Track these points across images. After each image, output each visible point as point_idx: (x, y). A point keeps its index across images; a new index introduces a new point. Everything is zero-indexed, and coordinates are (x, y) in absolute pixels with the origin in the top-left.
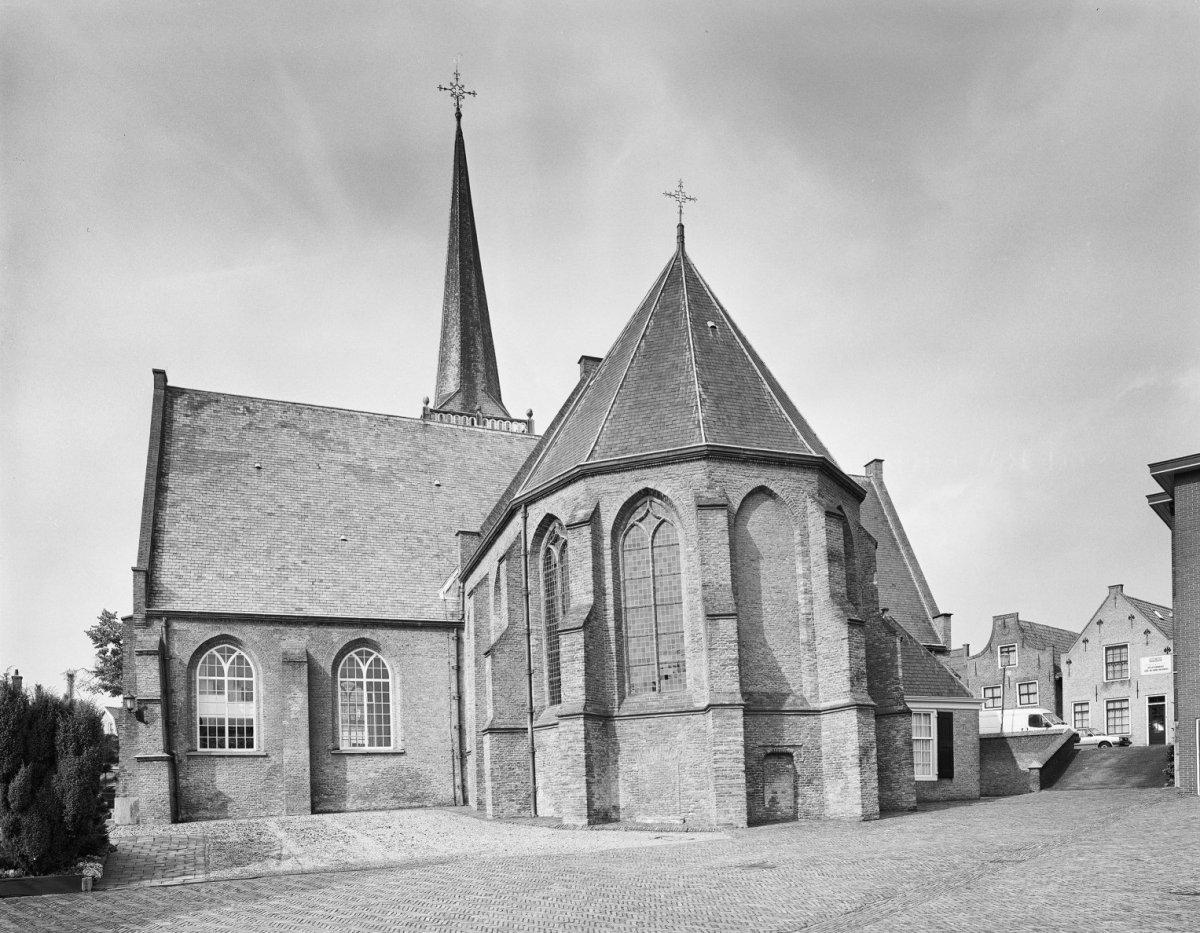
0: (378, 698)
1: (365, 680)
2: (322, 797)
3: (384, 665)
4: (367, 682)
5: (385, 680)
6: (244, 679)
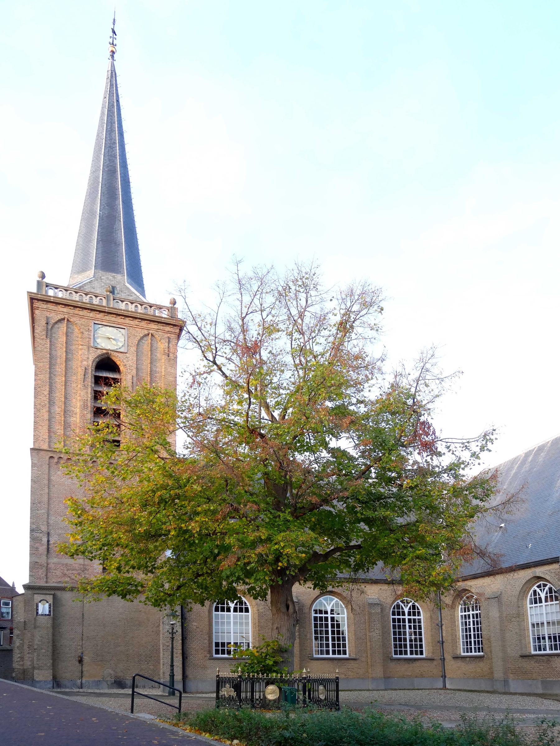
1: (407, 617)
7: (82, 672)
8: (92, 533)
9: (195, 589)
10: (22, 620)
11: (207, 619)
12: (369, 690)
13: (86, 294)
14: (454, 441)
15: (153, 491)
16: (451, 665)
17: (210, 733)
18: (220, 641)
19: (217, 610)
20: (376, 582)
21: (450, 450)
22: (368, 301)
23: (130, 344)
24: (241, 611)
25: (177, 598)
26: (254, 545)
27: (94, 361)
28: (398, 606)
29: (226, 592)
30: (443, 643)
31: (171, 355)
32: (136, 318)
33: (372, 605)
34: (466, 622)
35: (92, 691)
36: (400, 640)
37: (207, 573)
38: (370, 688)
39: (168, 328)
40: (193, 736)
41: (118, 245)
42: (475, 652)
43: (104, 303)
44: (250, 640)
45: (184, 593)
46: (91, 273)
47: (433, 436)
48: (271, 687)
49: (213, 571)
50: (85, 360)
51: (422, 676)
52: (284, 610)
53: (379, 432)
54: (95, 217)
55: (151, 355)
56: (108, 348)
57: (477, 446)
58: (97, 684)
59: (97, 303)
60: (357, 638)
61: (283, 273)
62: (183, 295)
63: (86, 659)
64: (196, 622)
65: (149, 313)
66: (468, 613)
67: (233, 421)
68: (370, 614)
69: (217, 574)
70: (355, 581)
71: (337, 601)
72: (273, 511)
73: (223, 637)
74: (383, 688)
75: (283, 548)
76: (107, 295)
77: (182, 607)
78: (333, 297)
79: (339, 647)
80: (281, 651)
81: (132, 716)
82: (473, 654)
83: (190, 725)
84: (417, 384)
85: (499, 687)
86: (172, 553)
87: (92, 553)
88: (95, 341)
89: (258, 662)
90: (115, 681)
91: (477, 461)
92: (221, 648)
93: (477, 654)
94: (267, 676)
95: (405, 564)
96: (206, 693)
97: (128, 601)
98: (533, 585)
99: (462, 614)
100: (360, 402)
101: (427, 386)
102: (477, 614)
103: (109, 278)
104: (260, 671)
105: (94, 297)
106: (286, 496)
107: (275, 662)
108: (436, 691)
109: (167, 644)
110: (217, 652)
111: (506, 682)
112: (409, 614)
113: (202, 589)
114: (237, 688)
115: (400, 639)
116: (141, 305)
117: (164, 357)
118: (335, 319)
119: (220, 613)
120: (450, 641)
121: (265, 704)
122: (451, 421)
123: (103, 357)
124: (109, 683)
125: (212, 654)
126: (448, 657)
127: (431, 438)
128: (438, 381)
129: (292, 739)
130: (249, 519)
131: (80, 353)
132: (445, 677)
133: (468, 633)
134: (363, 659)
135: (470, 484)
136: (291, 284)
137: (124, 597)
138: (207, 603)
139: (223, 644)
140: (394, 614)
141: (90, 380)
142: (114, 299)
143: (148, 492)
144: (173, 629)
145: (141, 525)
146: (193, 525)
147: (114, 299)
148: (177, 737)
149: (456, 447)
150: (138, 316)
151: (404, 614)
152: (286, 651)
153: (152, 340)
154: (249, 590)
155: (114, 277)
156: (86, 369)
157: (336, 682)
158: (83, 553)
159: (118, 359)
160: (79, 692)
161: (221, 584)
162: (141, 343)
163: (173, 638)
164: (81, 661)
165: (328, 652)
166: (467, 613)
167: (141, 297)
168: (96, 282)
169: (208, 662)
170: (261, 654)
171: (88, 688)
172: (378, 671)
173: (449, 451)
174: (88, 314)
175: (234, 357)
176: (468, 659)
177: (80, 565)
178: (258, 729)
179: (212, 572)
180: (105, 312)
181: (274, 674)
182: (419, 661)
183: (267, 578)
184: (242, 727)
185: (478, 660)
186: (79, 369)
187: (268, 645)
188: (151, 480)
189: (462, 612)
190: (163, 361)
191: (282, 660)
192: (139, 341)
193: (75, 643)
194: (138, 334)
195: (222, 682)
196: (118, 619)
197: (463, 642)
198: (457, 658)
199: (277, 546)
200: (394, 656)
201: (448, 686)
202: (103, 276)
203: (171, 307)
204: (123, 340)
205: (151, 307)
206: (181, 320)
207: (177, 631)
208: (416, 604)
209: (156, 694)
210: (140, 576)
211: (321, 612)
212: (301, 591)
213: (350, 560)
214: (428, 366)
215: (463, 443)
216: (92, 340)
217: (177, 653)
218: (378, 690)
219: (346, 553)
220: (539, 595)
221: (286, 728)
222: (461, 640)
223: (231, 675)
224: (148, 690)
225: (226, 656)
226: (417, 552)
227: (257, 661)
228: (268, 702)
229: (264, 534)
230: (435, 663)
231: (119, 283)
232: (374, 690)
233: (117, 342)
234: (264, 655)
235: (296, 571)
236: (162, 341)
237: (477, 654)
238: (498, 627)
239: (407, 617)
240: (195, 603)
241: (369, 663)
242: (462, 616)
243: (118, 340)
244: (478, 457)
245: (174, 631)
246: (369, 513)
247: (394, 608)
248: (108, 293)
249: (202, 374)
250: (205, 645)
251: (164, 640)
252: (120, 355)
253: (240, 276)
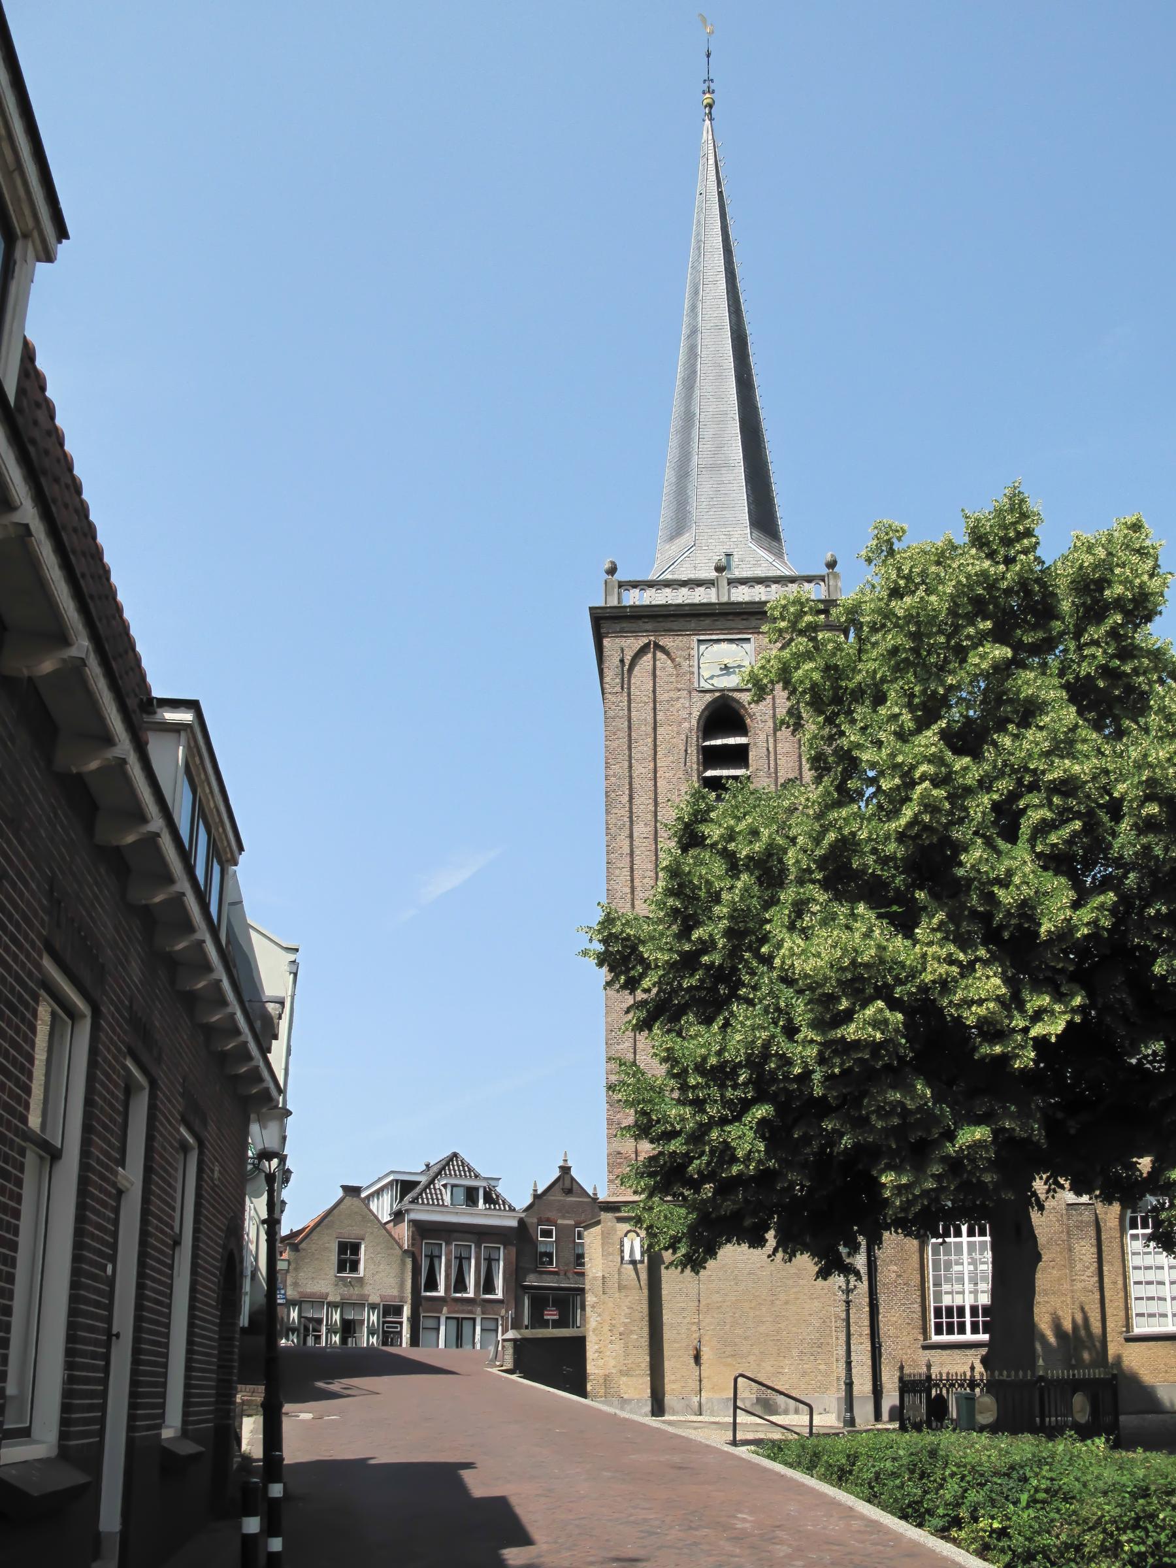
7: (700, 1381)
10: (600, 1274)
27: (700, 716)
90: (758, 1399)
164: (697, 1358)
165: (962, 1330)
193: (688, 1320)
196: (758, 1265)
216: (696, 675)
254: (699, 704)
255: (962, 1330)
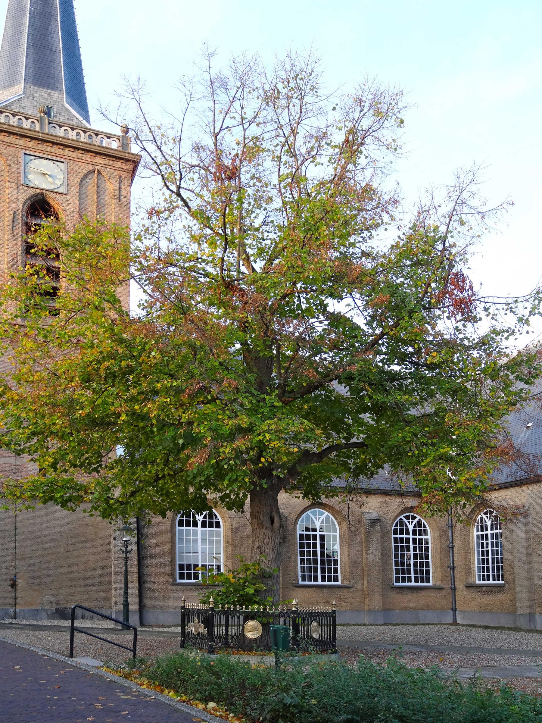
0: (421, 549)
1: (411, 536)
2: (71, 656)
3: (425, 527)
4: (320, 535)
5: (425, 537)
6: (331, 533)
7: (15, 599)
8: (19, 417)
9: (154, 496)
11: (169, 536)
12: (365, 625)
13: (14, 115)
14: (496, 300)
15: (98, 362)
16: (463, 596)
17: (175, 692)
18: (185, 563)
19: (181, 524)
20: (376, 492)
21: (489, 314)
22: (383, 109)
23: (71, 183)
24: (211, 526)
25: (131, 507)
26: (231, 437)
27: (25, 203)
28: (401, 523)
29: (193, 500)
30: (454, 569)
31: (123, 199)
32: (78, 149)
33: (370, 521)
34: (483, 544)
35: (28, 623)
36: (403, 564)
37: (169, 475)
38: (367, 623)
39: (118, 164)
40: (152, 694)
41: (54, 52)
42: (494, 580)
43: (37, 127)
44: (222, 561)
45: (140, 501)
46: (19, 88)
47: (470, 292)
48: (251, 623)
49: (176, 472)
50: (13, 202)
51: (428, 608)
52: (268, 524)
53: (394, 289)
54: (25, 15)
55: (97, 198)
56: (42, 187)
57: (526, 308)
58: (35, 613)
59: (28, 127)
60: (352, 562)
61: (270, 71)
62: (137, 98)
63: (20, 583)
64: (155, 539)
65: (95, 143)
66: (486, 532)
67: (204, 270)
68: (368, 532)
69: (182, 476)
70: (352, 491)
71: (327, 515)
72: (256, 393)
73: (188, 558)
74: (382, 622)
75: (270, 440)
76: (41, 117)
77: (138, 518)
78: (337, 105)
79: (330, 571)
80: (264, 576)
81: (69, 661)
82: (491, 582)
83: (148, 679)
84: (450, 220)
85: (523, 623)
86: (124, 451)
87: (20, 445)
88: (25, 176)
89: (236, 591)
91: (526, 328)
92: (188, 570)
93: (496, 582)
94: (247, 608)
95: (424, 466)
96: (169, 626)
97: (68, 510)
98: (480, 511)
99: (478, 533)
100: (366, 255)
101: (462, 223)
102: (497, 534)
103: (42, 96)
104: (237, 601)
105: (24, 119)
106: (271, 373)
107: (256, 591)
108: (446, 627)
109: (120, 566)
110: (181, 576)
111: (531, 617)
112: (414, 533)
113: (162, 495)
114: (208, 622)
115: (404, 563)
116: (85, 132)
117: (114, 202)
118: (339, 138)
119: (185, 528)
120: (463, 567)
121: (245, 645)
122: (493, 270)
123: (37, 198)
124: (49, 613)
125: (176, 578)
126: (460, 586)
127: (466, 295)
128: (479, 217)
129: (294, 706)
130: (224, 402)
131: (7, 192)
132: (456, 609)
133: (485, 557)
134: (359, 587)
135: (513, 360)
136: (280, 86)
137: (64, 504)
138: (169, 514)
139: (189, 566)
140: (396, 533)
141: (19, 228)
142: (49, 123)
143: (91, 362)
144: (127, 547)
145: (82, 408)
146: (150, 406)
147: (49, 123)
148: (129, 697)
149: (498, 309)
150: (81, 146)
151: (408, 533)
152: (270, 577)
153: (98, 179)
154: (222, 499)
155: (49, 94)
156: (14, 213)
157: (333, 617)
158: (8, 445)
159: (55, 202)
160: (11, 624)
161: (187, 490)
162: (85, 182)
163: (126, 559)
164: (13, 585)
165: (316, 579)
166: (484, 533)
167: (84, 122)
168: (26, 101)
169: (170, 588)
170: (238, 580)
171: (24, 618)
172: (377, 602)
173: (488, 315)
174: (17, 141)
175: (205, 192)
176: (484, 589)
177: (11, 465)
178: (242, 686)
179: (175, 474)
180: (37, 139)
181: (256, 607)
182: (426, 590)
183: (247, 480)
184: (220, 684)
185: (497, 590)
186: (7, 213)
187: (247, 569)
188: (95, 346)
189: (478, 531)
190: (113, 206)
191: (265, 588)
192: (83, 179)
193: (7, 563)
194: (80, 170)
195: (189, 615)
196: (59, 534)
197: (479, 568)
198: (471, 587)
199: (261, 437)
200: (395, 584)
201: (459, 621)
202: (36, 92)
203: (123, 136)
204: (62, 177)
205: (97, 135)
206: (137, 155)
207: (132, 550)
208: (423, 521)
209: (106, 627)
210: (83, 478)
211: (308, 529)
212: (288, 501)
213: (349, 462)
214: (465, 195)
215: (508, 304)
216: (22, 175)
217: (132, 577)
218: (376, 625)
219: (345, 453)
220: (486, 522)
221: (286, 690)
222: (476, 566)
223: (201, 606)
224: (97, 622)
225: (192, 581)
226: (441, 450)
227: (234, 589)
228: (247, 642)
229: (244, 420)
230: (444, 592)
231: (56, 102)
232: (371, 625)
233: (54, 180)
234: (242, 581)
235: (286, 472)
236: (112, 180)
237: (496, 582)
238: (524, 550)
239: (411, 536)
240: (154, 513)
241: (366, 592)
242: (478, 536)
243: (56, 177)
244: (527, 322)
245: (129, 549)
246: (379, 397)
247: (396, 525)
248: (42, 115)
249: (162, 213)
250: (167, 568)
251: (116, 560)
252: (58, 197)
253: (213, 75)
254: (23, 196)
255: (409, 580)
